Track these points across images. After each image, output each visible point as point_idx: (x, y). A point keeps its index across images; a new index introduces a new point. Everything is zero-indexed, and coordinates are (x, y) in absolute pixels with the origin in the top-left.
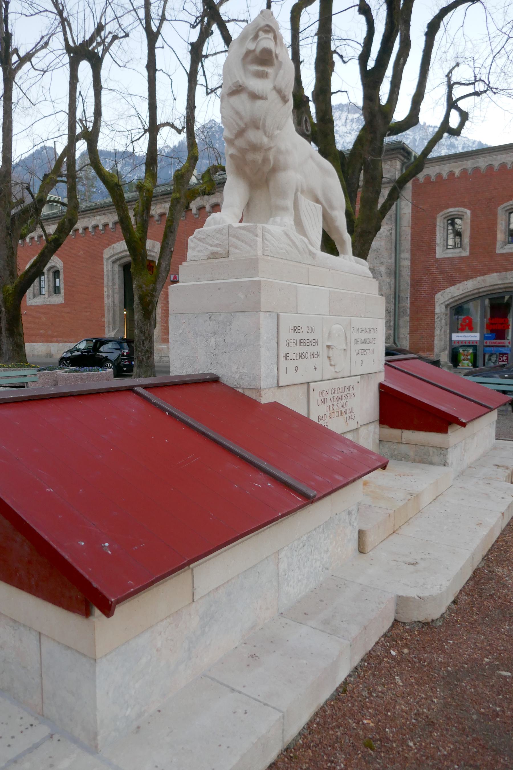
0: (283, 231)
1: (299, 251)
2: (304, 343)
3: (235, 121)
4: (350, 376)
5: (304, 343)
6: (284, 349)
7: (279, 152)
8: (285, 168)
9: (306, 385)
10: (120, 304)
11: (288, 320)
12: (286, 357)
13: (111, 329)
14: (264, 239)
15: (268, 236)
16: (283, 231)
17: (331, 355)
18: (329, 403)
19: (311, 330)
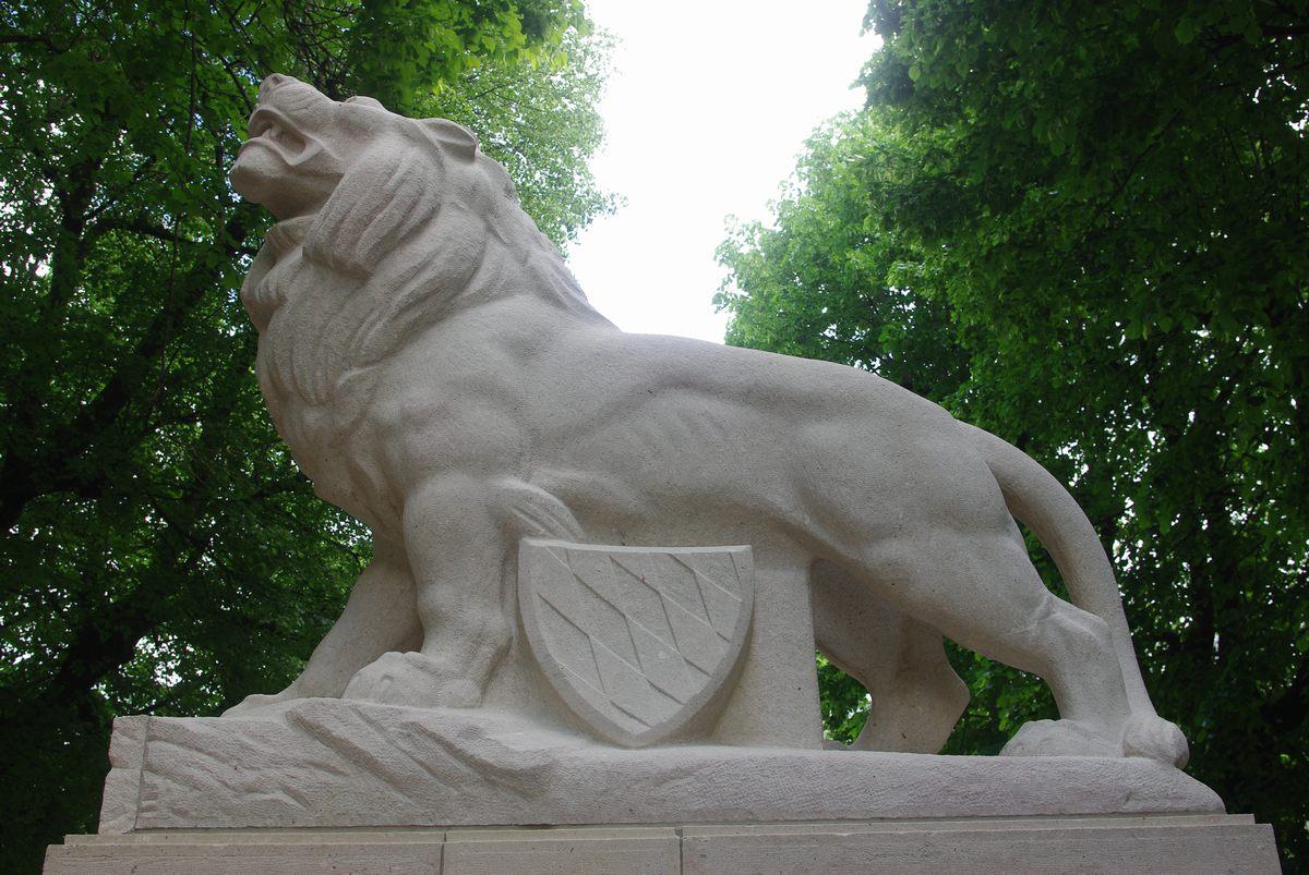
1: (393, 781)
7: (383, 432)
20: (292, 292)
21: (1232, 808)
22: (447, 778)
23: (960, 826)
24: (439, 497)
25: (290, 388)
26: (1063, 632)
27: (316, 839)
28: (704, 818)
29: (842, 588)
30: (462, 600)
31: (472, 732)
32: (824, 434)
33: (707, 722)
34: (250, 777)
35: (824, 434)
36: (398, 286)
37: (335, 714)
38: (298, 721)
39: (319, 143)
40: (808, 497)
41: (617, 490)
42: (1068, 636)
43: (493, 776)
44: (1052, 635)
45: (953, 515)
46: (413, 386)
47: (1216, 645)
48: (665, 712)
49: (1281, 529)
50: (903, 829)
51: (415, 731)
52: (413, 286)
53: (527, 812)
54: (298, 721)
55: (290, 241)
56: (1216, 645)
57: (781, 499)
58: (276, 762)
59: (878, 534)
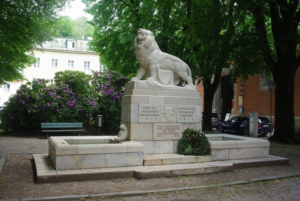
0: (146, 82)
1: (153, 86)
2: (155, 112)
3: (152, 48)
4: (177, 123)
5: (155, 112)
6: (140, 113)
7: (148, 60)
8: (151, 64)
9: (152, 124)
10: (219, 95)
11: (142, 105)
12: (142, 115)
13: (214, 108)
14: (137, 85)
15: (138, 84)
16: (146, 82)
17: (165, 116)
18: (163, 130)
19: (155, 108)
20: (142, 48)
21: (198, 91)
22: (156, 87)
23: (184, 92)
24: (153, 66)
25: (141, 55)
26: (189, 79)
27: (149, 90)
28: (170, 90)
29: (175, 74)
30: (154, 73)
31: (157, 84)
32: (177, 63)
33: (168, 84)
34: (144, 86)
35: (177, 63)
36: (150, 49)
37: (149, 81)
38: (146, 82)
39: (145, 35)
40: (176, 69)
41: (163, 66)
42: (189, 79)
43: (158, 86)
44: (188, 79)
45: (184, 70)
46: (151, 58)
47: (213, 76)
48: (167, 83)
49: (249, 11)
50: (181, 92)
51: (154, 83)
52: (151, 49)
53: (160, 89)
54: (146, 82)
55: (142, 43)
56: (213, 76)
57: (173, 67)
58: (145, 85)
59: (179, 71)
